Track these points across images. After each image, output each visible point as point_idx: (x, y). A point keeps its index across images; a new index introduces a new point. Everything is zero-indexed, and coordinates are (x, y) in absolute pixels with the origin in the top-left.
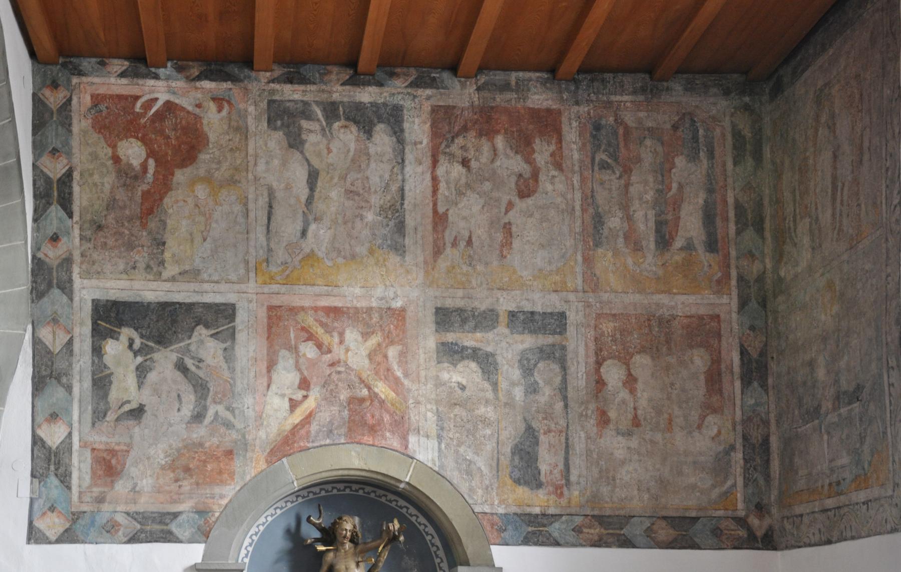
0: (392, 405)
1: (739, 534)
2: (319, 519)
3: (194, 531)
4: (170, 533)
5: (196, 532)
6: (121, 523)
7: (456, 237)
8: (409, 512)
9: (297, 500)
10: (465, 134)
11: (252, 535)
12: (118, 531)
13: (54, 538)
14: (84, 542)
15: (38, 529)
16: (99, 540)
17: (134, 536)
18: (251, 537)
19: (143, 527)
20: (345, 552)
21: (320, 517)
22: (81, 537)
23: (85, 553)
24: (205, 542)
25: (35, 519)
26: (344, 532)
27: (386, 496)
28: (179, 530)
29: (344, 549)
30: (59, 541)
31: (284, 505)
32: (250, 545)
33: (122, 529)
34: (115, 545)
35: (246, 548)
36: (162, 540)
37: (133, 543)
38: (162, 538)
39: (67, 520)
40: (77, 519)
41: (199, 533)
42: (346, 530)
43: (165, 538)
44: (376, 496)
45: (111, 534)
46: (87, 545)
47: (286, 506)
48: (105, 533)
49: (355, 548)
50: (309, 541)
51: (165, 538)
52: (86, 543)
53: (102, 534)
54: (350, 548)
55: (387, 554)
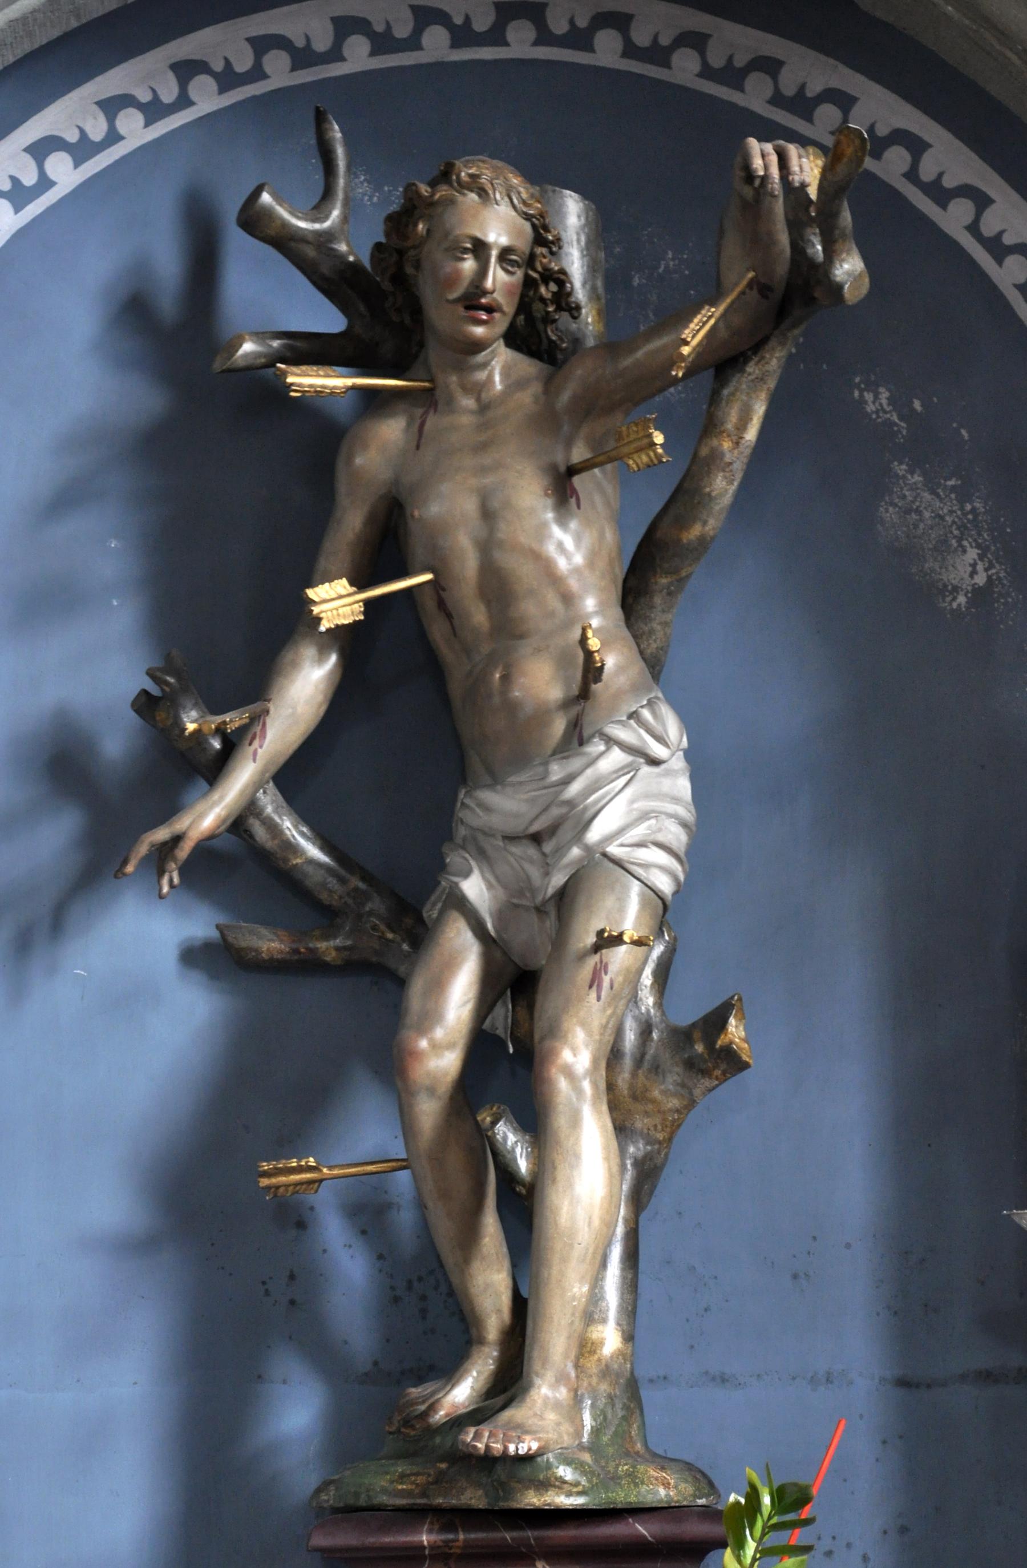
1: (605, 1434)
2: (319, 209)
8: (927, 171)
9: (184, 102)
10: (837, 232)
20: (484, 408)
21: (328, 194)
26: (469, 265)
27: (770, 66)
29: (477, 390)
31: (97, 129)
42: (480, 248)
44: (707, 72)
47: (113, 137)
49: (550, 385)
50: (248, 347)
54: (515, 385)
55: (760, 409)
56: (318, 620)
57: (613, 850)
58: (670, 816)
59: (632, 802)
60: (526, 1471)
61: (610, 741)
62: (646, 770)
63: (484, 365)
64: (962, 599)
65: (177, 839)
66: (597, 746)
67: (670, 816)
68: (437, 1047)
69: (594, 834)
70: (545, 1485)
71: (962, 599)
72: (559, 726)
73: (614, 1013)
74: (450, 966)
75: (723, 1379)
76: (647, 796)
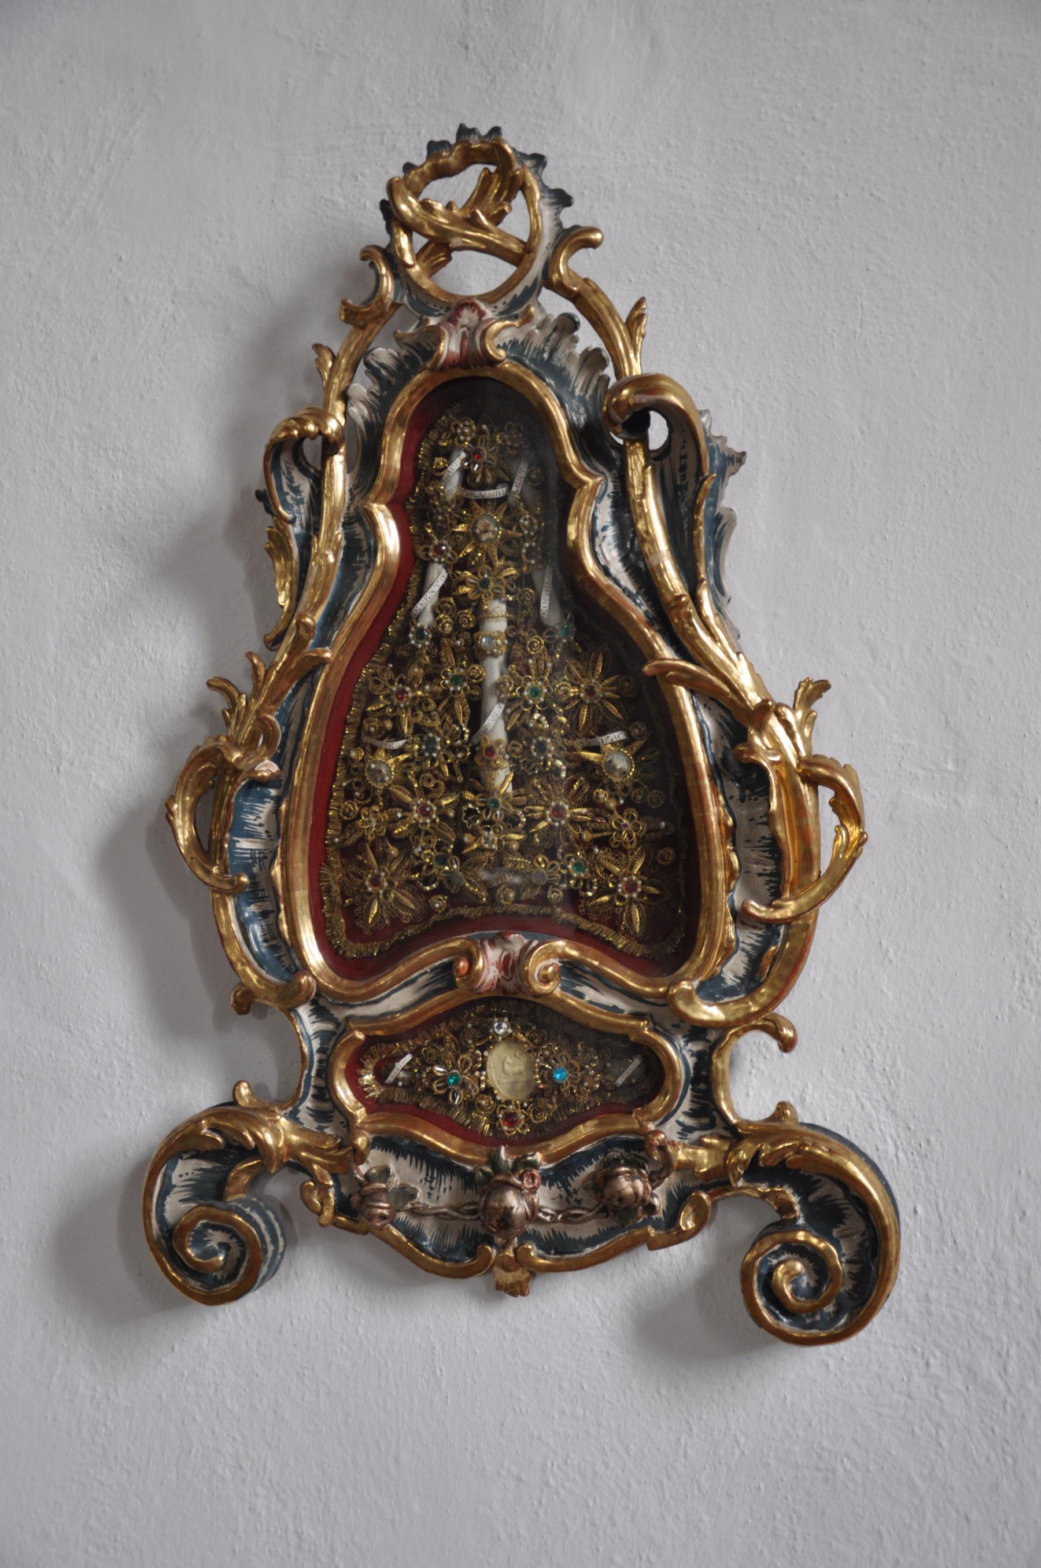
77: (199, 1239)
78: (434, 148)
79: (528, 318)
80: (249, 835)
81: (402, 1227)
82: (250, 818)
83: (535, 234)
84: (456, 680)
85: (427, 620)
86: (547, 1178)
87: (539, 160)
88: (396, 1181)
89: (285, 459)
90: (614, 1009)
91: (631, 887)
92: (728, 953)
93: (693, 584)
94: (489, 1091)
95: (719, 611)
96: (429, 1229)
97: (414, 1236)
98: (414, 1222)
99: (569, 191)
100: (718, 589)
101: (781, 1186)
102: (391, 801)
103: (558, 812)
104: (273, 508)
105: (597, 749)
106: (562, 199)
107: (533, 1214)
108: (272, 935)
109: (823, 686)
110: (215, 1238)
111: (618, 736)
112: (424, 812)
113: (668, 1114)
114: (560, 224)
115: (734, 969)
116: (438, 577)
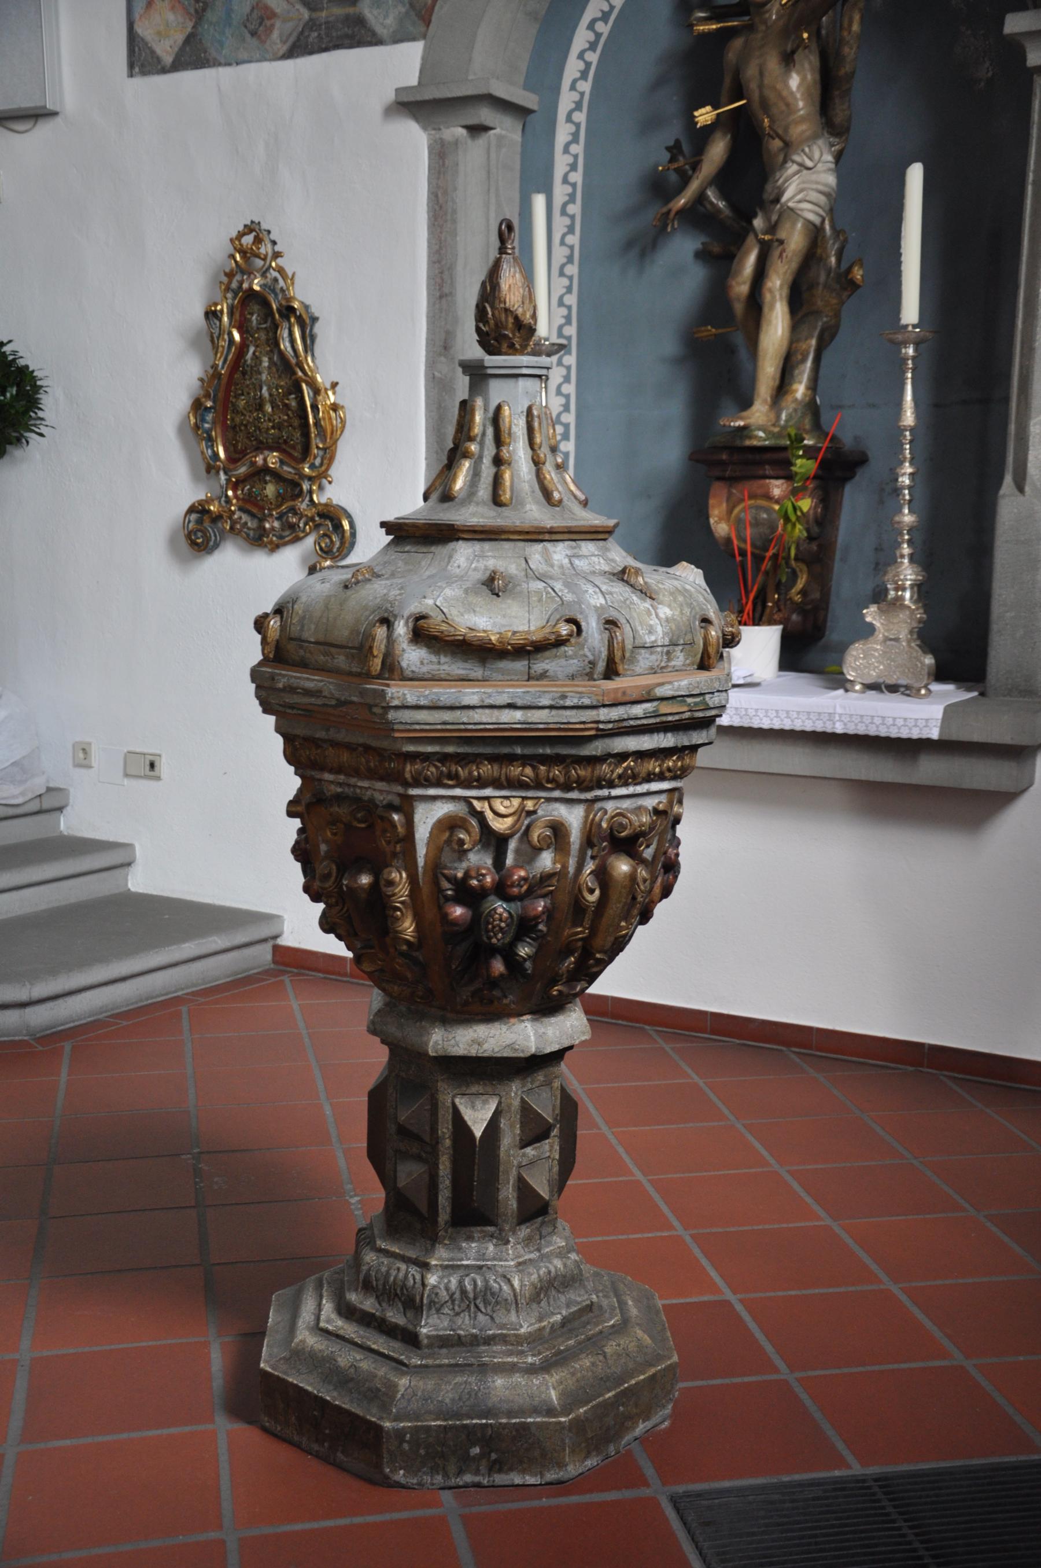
0: (440, 587)
3: (403, 10)
4: (360, 21)
5: (407, 13)
6: (278, 11)
7: (529, 411)
11: (593, 21)
12: (270, 30)
13: (168, 59)
14: (216, 64)
15: (143, 39)
16: (243, 55)
17: (298, 39)
18: (591, 26)
19: (315, 15)
22: (213, 53)
23: (219, 89)
24: (424, 37)
25: (137, 16)
28: (375, 12)
29: (765, 22)
30: (178, 65)
32: (593, 46)
33: (278, 24)
34: (266, 65)
35: (581, 56)
36: (347, 42)
37: (297, 56)
38: (347, 36)
39: (188, 13)
40: (204, 10)
41: (412, 13)
43: (351, 37)
45: (259, 38)
46: (221, 69)
48: (248, 36)
51: (351, 37)
52: (220, 64)
53: (244, 40)
56: (697, 123)
57: (790, 204)
58: (813, 189)
59: (798, 185)
60: (745, 433)
61: (793, 162)
62: (805, 172)
63: (767, 12)
64: (982, 84)
65: (669, 211)
66: (789, 164)
67: (813, 189)
68: (739, 284)
69: (784, 199)
70: (750, 437)
71: (982, 84)
72: (781, 158)
73: (788, 268)
74: (747, 253)
75: (874, 406)
76: (804, 182)
77: (195, 534)
78: (245, 226)
79: (266, 277)
80: (208, 423)
81: (246, 533)
82: (207, 418)
83: (267, 253)
84: (256, 379)
85: (249, 362)
86: (277, 519)
87: (269, 232)
88: (243, 521)
89: (210, 316)
90: (290, 473)
91: (297, 439)
92: (315, 458)
93: (306, 351)
94: (267, 496)
95: (313, 361)
96: (251, 533)
97: (248, 535)
98: (248, 531)
99: (277, 240)
100: (313, 356)
101: (921, 590)
102: (243, 414)
103: (280, 418)
104: (609, 530)
105: (288, 399)
106: (274, 243)
107: (273, 529)
108: (213, 451)
109: (337, 384)
110: (199, 534)
111: (293, 396)
112: (250, 417)
113: (303, 501)
114: (273, 250)
115: (318, 462)
116: (252, 349)
